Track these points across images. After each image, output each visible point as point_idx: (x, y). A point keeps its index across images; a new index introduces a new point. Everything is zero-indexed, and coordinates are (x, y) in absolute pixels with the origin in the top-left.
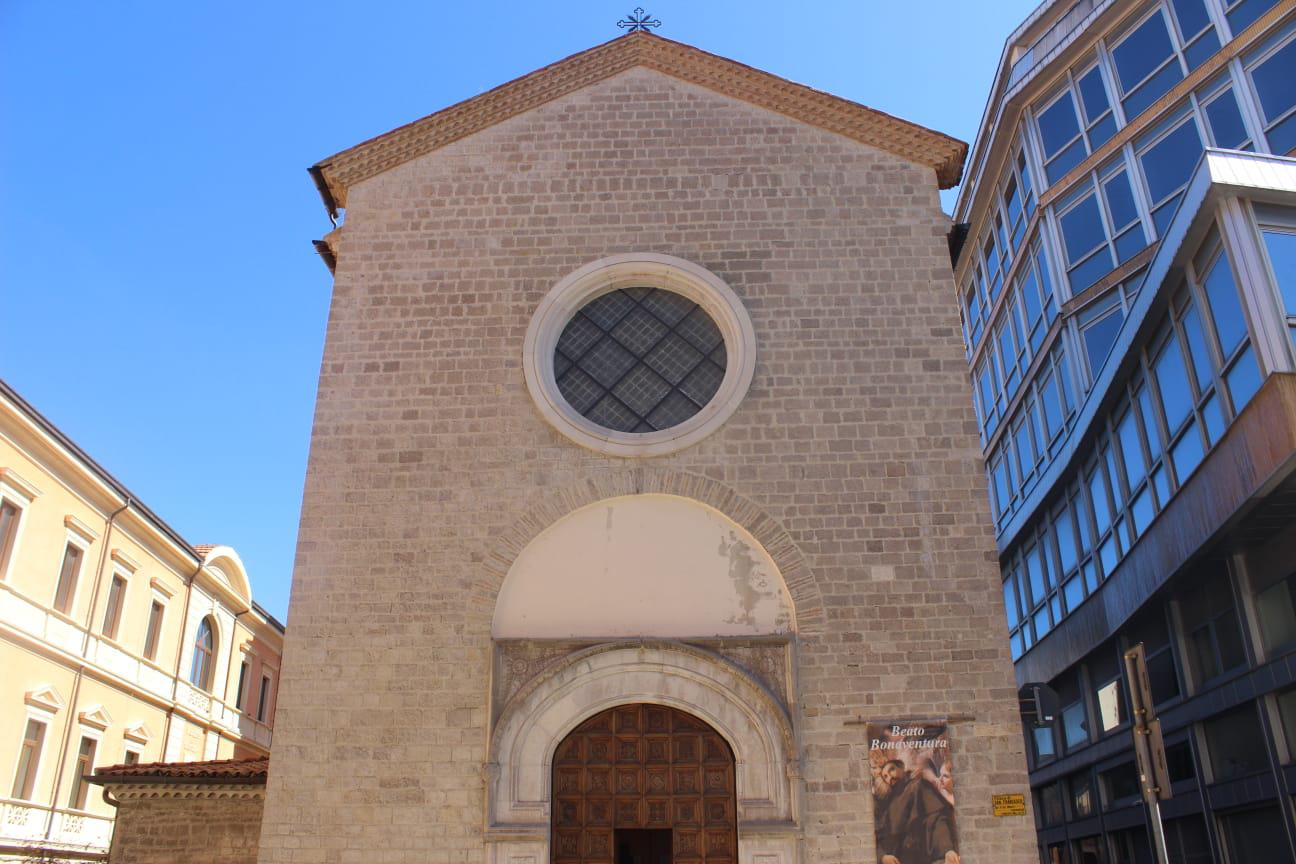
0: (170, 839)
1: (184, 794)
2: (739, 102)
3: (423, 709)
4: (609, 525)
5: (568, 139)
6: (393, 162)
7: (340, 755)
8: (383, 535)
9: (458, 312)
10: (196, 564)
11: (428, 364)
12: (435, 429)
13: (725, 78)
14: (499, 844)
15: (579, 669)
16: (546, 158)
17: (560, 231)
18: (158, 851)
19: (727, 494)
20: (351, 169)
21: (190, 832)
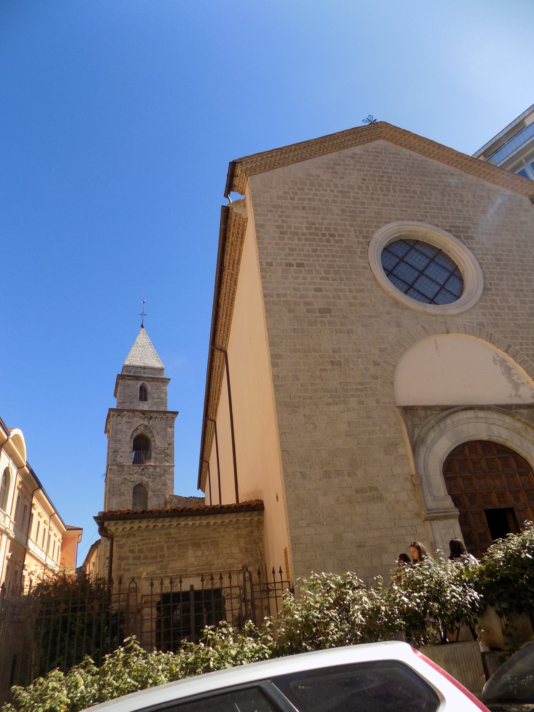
0: (152, 555)
1: (160, 525)
2: (433, 160)
3: (369, 446)
4: (437, 349)
5: (358, 167)
6: (271, 167)
7: (327, 475)
8: (321, 351)
9: (328, 241)
10: (6, 437)
11: (320, 265)
12: (334, 297)
13: (426, 149)
14: (432, 522)
15: (447, 421)
16: (350, 174)
17: (368, 208)
18: (145, 563)
19: (489, 335)
20: (252, 166)
21: (165, 549)
